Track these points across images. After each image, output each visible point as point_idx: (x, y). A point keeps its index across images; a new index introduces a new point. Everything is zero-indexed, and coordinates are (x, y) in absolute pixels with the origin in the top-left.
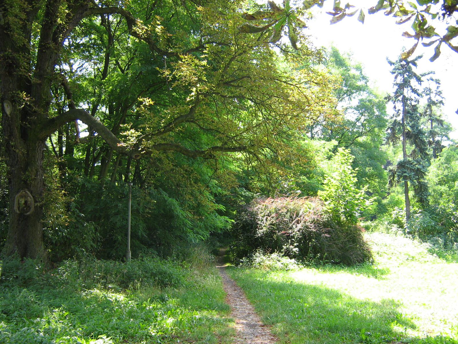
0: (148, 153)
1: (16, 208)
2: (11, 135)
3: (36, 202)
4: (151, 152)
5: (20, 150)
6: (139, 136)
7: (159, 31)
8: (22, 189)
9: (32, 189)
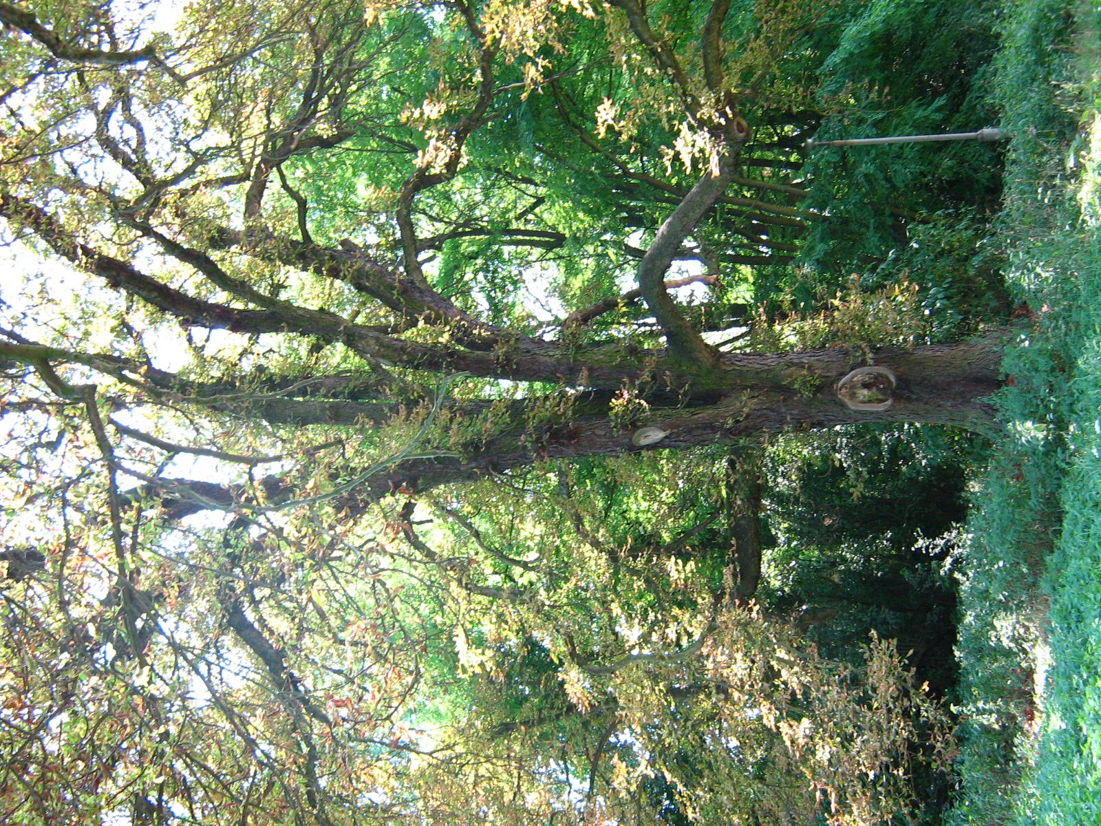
0: (731, 100)
1: (881, 407)
2: (710, 427)
3: (863, 363)
4: (728, 93)
5: (745, 403)
6: (691, 128)
7: (436, 109)
8: (835, 395)
9: (833, 374)
